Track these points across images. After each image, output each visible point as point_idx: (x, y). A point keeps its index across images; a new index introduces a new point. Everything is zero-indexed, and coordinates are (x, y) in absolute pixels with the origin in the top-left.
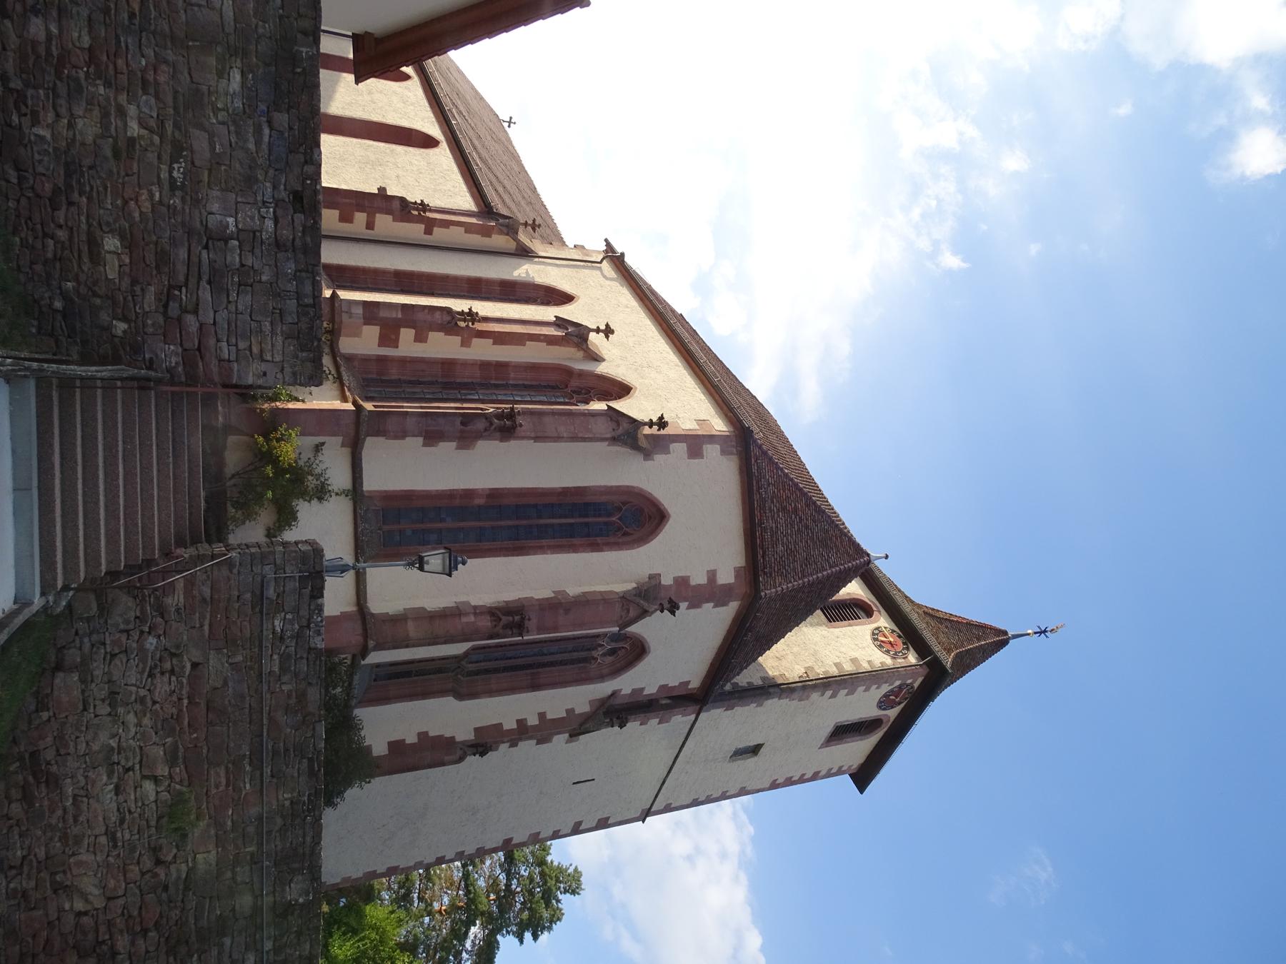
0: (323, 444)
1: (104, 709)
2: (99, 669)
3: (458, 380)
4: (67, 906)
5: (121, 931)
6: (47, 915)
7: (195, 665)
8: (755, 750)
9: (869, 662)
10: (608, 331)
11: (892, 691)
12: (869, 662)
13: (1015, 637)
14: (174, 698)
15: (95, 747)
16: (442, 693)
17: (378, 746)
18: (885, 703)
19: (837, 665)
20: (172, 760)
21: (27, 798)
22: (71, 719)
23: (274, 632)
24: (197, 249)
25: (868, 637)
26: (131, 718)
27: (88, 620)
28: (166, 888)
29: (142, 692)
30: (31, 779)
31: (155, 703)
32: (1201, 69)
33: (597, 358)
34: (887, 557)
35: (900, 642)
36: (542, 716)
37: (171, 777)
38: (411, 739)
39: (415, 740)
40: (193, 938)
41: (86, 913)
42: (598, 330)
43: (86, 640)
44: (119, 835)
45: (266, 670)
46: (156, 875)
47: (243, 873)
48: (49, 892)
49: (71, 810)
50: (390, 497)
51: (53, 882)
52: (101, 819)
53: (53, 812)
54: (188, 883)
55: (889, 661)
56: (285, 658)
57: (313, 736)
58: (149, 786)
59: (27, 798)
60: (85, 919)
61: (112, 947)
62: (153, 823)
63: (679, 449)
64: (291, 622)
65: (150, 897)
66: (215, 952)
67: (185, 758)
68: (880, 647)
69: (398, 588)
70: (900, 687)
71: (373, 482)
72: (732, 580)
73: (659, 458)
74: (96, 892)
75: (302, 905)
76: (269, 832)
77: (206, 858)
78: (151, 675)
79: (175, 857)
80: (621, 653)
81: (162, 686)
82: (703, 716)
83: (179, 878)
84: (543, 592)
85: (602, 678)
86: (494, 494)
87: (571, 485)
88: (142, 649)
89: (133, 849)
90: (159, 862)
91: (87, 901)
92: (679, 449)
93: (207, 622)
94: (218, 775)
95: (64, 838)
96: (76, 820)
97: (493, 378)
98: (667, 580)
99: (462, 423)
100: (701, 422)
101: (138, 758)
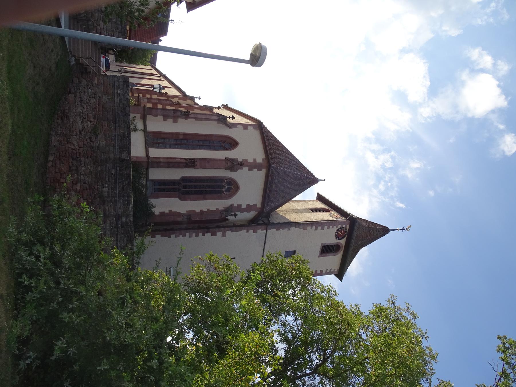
0: (135, 117)
1: (79, 104)
2: (78, 94)
7: (100, 97)
11: (338, 230)
18: (338, 236)
20: (94, 117)
24: (99, 14)
26: (85, 107)
27: (76, 84)
28: (93, 148)
32: (471, 121)
34: (257, 58)
41: (74, 149)
47: (111, 148)
50: (154, 133)
51: (67, 140)
53: (67, 124)
56: (120, 100)
58: (89, 123)
59: (62, 119)
60: (74, 151)
61: (80, 159)
65: (89, 149)
66: (105, 167)
69: (155, 153)
70: (341, 228)
71: (150, 128)
73: (234, 129)
78: (90, 98)
81: (92, 101)
85: (226, 198)
86: (185, 134)
89: (85, 136)
90: (91, 141)
95: (70, 130)
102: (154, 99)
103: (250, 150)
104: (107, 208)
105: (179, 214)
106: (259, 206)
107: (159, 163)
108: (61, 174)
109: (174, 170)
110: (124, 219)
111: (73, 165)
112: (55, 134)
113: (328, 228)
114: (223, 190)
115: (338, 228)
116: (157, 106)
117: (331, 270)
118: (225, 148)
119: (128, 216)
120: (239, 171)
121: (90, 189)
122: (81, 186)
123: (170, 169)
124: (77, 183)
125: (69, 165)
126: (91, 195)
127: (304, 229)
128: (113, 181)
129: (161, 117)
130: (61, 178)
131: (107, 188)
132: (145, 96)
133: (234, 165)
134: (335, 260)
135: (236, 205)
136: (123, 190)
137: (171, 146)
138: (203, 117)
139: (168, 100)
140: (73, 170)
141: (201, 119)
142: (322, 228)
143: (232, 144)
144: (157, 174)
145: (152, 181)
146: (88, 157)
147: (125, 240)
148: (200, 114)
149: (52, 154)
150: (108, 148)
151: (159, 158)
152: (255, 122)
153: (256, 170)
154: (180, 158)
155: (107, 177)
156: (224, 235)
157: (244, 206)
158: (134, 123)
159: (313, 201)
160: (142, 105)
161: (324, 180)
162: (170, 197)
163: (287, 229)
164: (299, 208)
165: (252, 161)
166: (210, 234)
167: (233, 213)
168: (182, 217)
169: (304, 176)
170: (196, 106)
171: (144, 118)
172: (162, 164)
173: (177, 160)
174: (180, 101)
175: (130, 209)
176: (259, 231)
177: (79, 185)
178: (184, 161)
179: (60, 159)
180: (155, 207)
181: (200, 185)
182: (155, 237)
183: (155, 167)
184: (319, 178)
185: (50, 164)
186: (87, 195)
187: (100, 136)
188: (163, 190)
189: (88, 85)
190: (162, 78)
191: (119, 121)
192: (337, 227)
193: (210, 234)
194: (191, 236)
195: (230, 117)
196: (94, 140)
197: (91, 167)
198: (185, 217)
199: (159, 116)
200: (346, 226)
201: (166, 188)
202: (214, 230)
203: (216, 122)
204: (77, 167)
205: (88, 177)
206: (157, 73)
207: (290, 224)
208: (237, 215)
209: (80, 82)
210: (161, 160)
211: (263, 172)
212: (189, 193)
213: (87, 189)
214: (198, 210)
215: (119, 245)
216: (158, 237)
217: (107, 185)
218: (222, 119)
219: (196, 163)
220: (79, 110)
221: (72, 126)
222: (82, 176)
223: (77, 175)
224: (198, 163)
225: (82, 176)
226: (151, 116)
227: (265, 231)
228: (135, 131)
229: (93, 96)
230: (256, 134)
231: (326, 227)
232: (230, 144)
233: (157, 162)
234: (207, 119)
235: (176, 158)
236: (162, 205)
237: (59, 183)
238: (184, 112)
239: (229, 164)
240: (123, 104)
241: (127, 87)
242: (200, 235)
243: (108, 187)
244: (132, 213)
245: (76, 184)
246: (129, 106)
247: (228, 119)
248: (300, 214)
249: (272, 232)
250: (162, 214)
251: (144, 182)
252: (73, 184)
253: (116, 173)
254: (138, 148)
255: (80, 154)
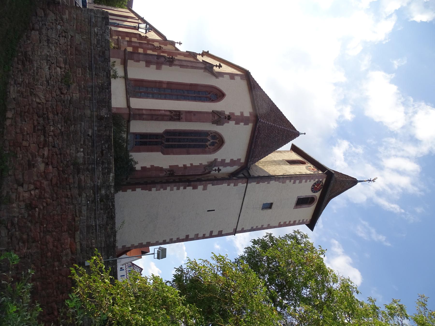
0: (115, 62)
1: (46, 44)
2: (44, 31)
4: (34, 100)
5: (50, 112)
6: (28, 101)
7: (72, 37)
11: (315, 183)
14: (66, 45)
15: (43, 54)
16: (157, 151)
18: (314, 189)
20: (65, 63)
21: (24, 65)
22: (36, 44)
23: (95, 32)
26: (53, 48)
27: (41, 17)
29: (57, 41)
30: (24, 59)
31: (60, 44)
36: (191, 164)
37: (65, 68)
39: (150, 167)
40: (72, 120)
41: (40, 104)
43: (41, 23)
44: (50, 82)
45: (93, 42)
46: (61, 96)
47: (87, 103)
48: (29, 94)
49: (36, 71)
51: (30, 91)
52: (44, 76)
53: (30, 70)
54: (70, 102)
56: (98, 40)
57: (107, 66)
58: (58, 69)
60: (40, 106)
61: (48, 116)
62: (60, 80)
64: (100, 30)
65: (59, 103)
66: (79, 126)
67: (69, 63)
69: (138, 103)
71: (131, 75)
72: (249, 115)
73: (221, 78)
74: (43, 97)
75: (106, 118)
76: (95, 92)
77: (76, 96)
78: (59, 37)
79: (66, 93)
80: (216, 145)
81: (62, 41)
82: (249, 185)
83: (68, 99)
85: (210, 153)
86: (169, 83)
88: (56, 29)
89: (54, 87)
90: (62, 93)
91: (40, 99)
93: (75, 25)
94: (79, 70)
95: (34, 79)
96: (37, 74)
99: (157, 59)
101: (55, 61)
102: (135, 42)
103: (236, 102)
104: (82, 178)
105: (161, 169)
106: (243, 161)
107: (140, 115)
108: (23, 135)
109: (158, 122)
110: (103, 192)
111: (39, 123)
112: (15, 83)
113: (306, 182)
114: (207, 144)
115: (315, 182)
116: (138, 50)
117: (303, 220)
118: (210, 99)
119: (108, 187)
120: (226, 124)
121: (60, 154)
122: (49, 150)
123: (154, 121)
124: (44, 146)
125: (33, 124)
126: (62, 162)
127: (283, 183)
128: (90, 144)
129: (143, 63)
130: (23, 140)
131: (82, 154)
132: (125, 39)
133: (219, 118)
134: (307, 211)
135: (219, 160)
136: (102, 154)
137: (154, 96)
138: (189, 64)
139: (148, 44)
140: (38, 130)
141: (187, 67)
142: (300, 182)
143: (217, 95)
144: (138, 127)
145: (134, 134)
146: (58, 114)
147: (105, 217)
148: (185, 61)
149: (11, 110)
150: (83, 102)
151: (142, 109)
152: (242, 72)
153: (243, 124)
154: (164, 110)
155: (82, 139)
156: (205, 189)
157: (228, 161)
158: (114, 68)
159: (288, 151)
160: (123, 49)
161: (305, 134)
162: (152, 151)
163: (267, 183)
164: (276, 159)
165: (239, 114)
166: (191, 188)
167: (217, 168)
168: (165, 173)
169: (288, 130)
170: (177, 52)
171: (125, 64)
172: (144, 117)
173: (161, 112)
174: (162, 46)
175: (111, 178)
176: (240, 185)
177: (46, 149)
178: (168, 113)
179: (21, 116)
180: (136, 163)
181: (184, 139)
182: (135, 190)
183: (137, 120)
184: (300, 132)
185: (8, 122)
186: (58, 163)
187: (73, 86)
188: (145, 144)
189: (56, 20)
190: (140, 21)
191: (96, 68)
192: (314, 180)
193: (191, 188)
194: (172, 190)
195: (216, 66)
196: (65, 92)
197: (62, 126)
198: (168, 173)
199: (141, 62)
200: (323, 180)
201: (147, 142)
202: (195, 183)
203: (202, 71)
204: (43, 126)
205: (58, 139)
206: (134, 16)
207: (269, 178)
208: (220, 170)
209: (46, 15)
210: (144, 112)
211: (250, 126)
212: (172, 146)
213: (56, 154)
214: (181, 165)
215: (98, 223)
216: (139, 190)
217: (82, 150)
218: (208, 68)
219: (182, 116)
220: (45, 52)
221: (37, 73)
222: (50, 138)
223: (45, 136)
224: (183, 116)
225: (50, 138)
226: (133, 61)
227: (245, 184)
228: (115, 78)
229: (64, 34)
230: (243, 85)
231: (304, 181)
232: (216, 95)
233: (139, 115)
234: (193, 67)
235: (160, 110)
236: (144, 160)
237: (20, 147)
238: (169, 58)
239: (216, 118)
240: (102, 46)
241: (106, 25)
242: (182, 188)
243: (83, 152)
244: (113, 184)
245: (43, 148)
246: (109, 49)
247: (215, 68)
248: (278, 166)
249: (252, 185)
250: (144, 168)
251: (125, 136)
252: (40, 148)
253: (93, 133)
254: (118, 99)
255: (47, 109)
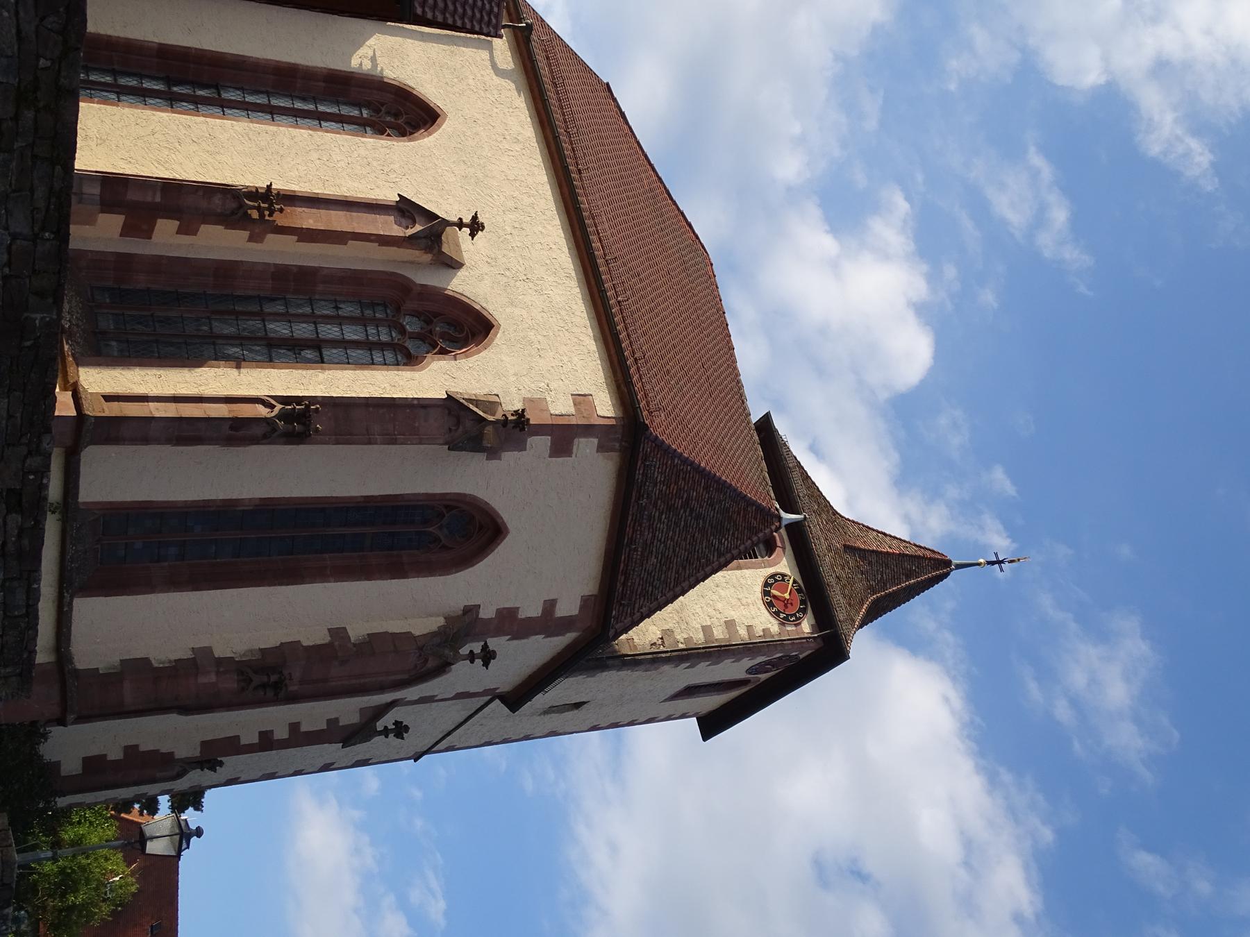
3: (238, 293)
8: (578, 705)
9: (749, 628)
10: (475, 226)
12: (749, 628)
13: (959, 566)
17: (71, 766)
19: (706, 629)
25: (758, 589)
33: (454, 265)
35: (798, 597)
38: (115, 754)
42: (460, 224)
55: (774, 626)
63: (540, 443)
68: (769, 605)
84: (315, 636)
87: (376, 493)
92: (540, 443)
97: (296, 284)
98: (487, 613)
99: (231, 428)
100: (581, 400)
